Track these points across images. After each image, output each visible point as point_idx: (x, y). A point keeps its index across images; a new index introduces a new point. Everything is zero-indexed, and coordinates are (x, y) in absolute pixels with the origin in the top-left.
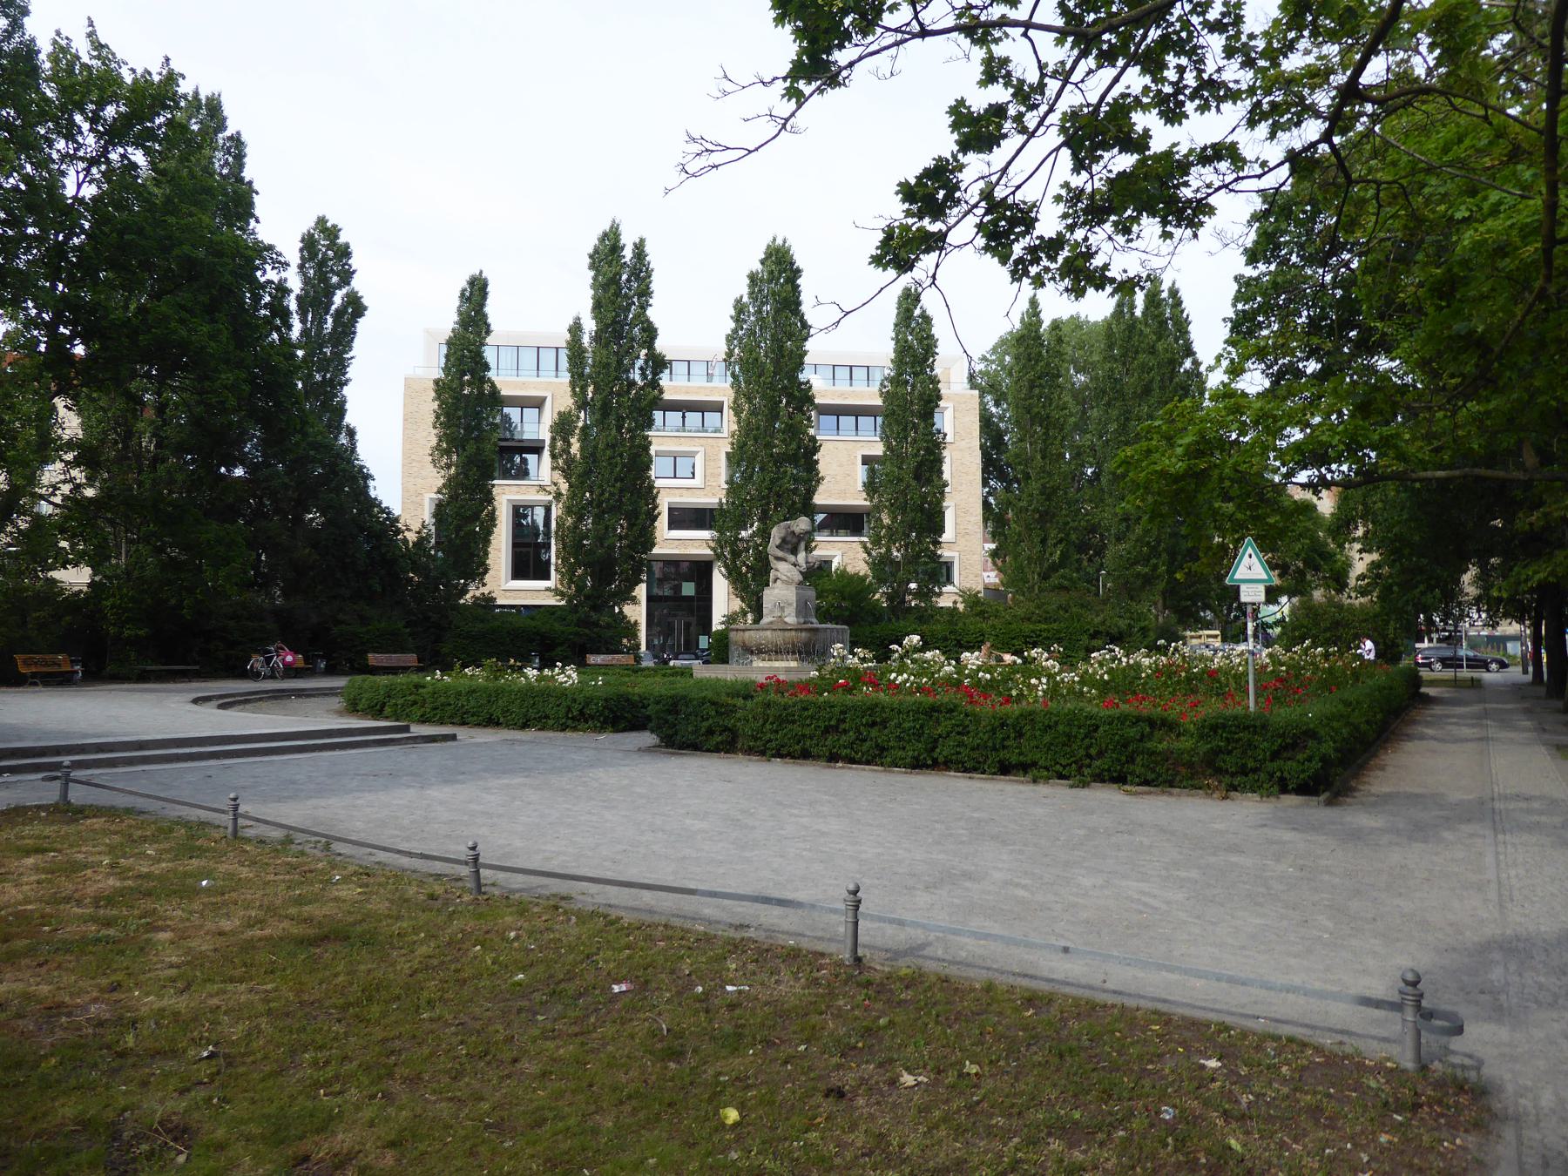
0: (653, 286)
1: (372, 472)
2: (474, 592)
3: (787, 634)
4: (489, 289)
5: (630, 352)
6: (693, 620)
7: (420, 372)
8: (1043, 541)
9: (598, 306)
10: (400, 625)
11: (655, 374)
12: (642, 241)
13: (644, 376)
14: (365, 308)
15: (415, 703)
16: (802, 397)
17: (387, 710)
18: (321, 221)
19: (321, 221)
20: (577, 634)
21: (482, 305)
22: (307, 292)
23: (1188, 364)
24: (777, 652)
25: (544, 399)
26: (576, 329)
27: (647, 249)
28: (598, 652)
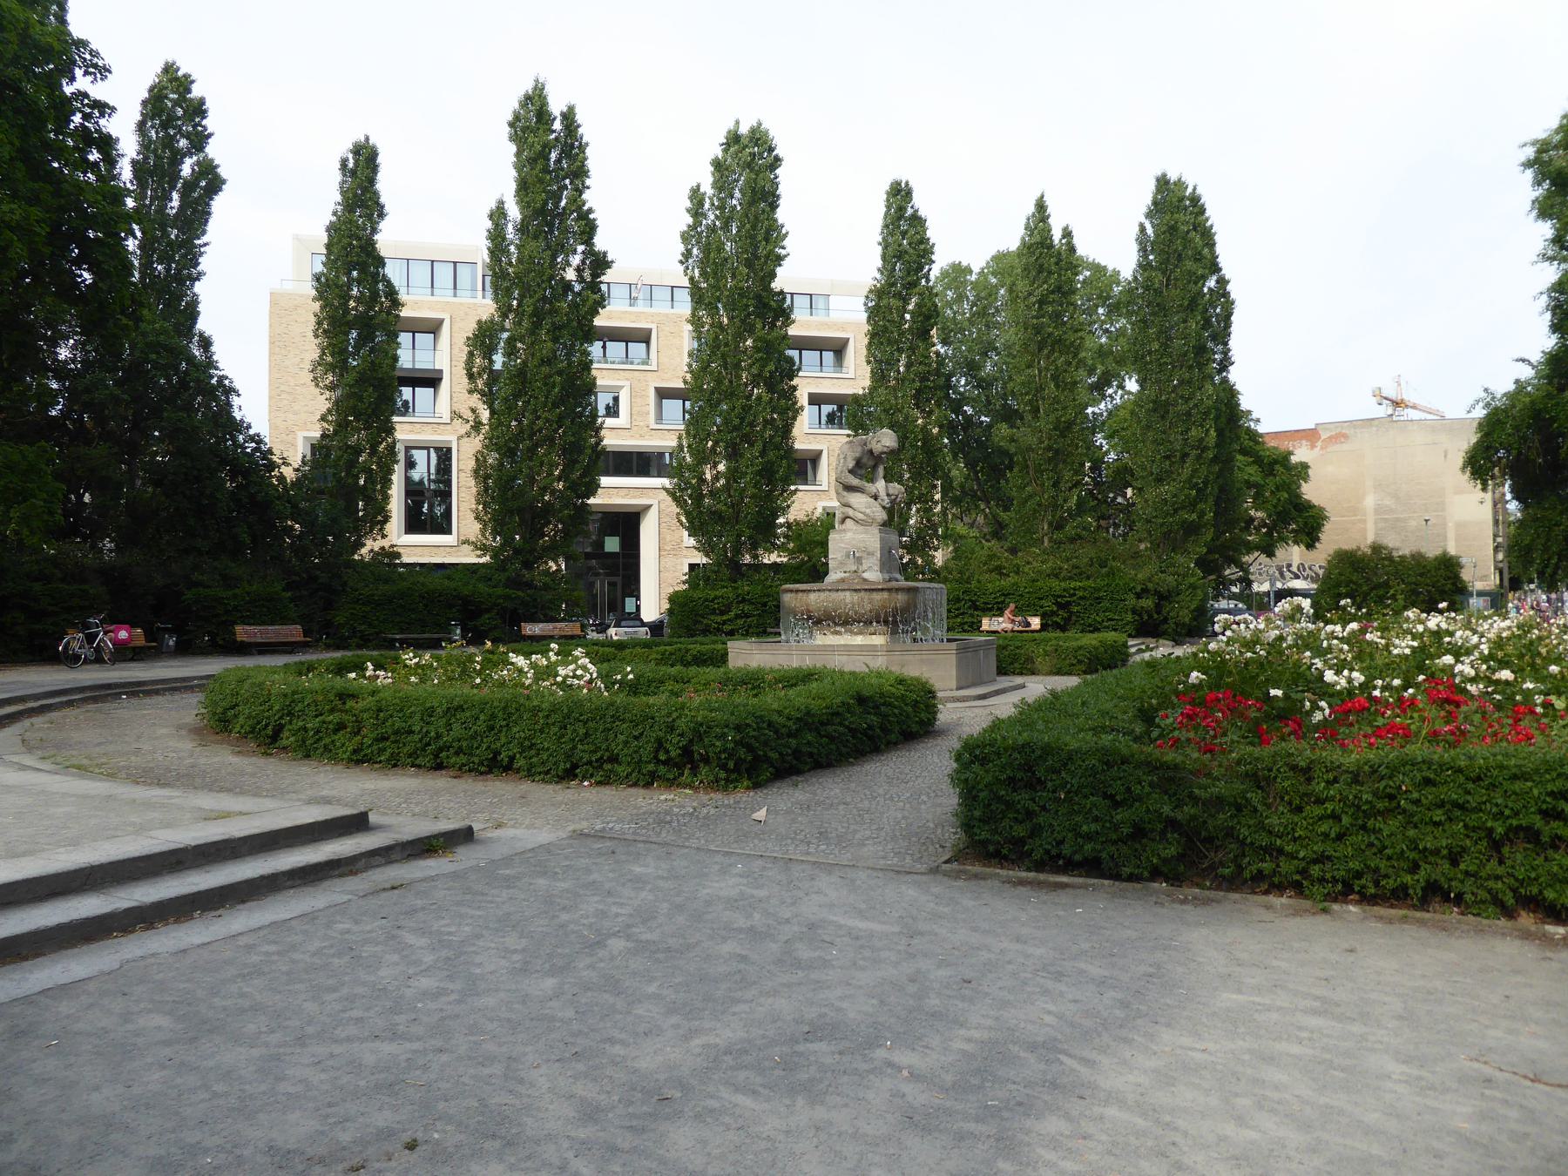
0: (590, 164)
1: (237, 385)
2: (371, 545)
3: (877, 596)
4: (379, 160)
5: (564, 249)
6: (618, 580)
7: (289, 287)
8: (1056, 484)
9: (523, 187)
10: (278, 587)
11: (595, 275)
12: (571, 109)
13: (581, 279)
14: (224, 182)
15: (341, 726)
16: (776, 309)
17: (287, 739)
18: (169, 69)
19: (169, 69)
20: (507, 597)
21: (372, 181)
22: (146, 158)
23: (1212, 283)
24: (866, 621)
25: (440, 322)
26: (498, 215)
27: (579, 118)
28: (533, 619)
